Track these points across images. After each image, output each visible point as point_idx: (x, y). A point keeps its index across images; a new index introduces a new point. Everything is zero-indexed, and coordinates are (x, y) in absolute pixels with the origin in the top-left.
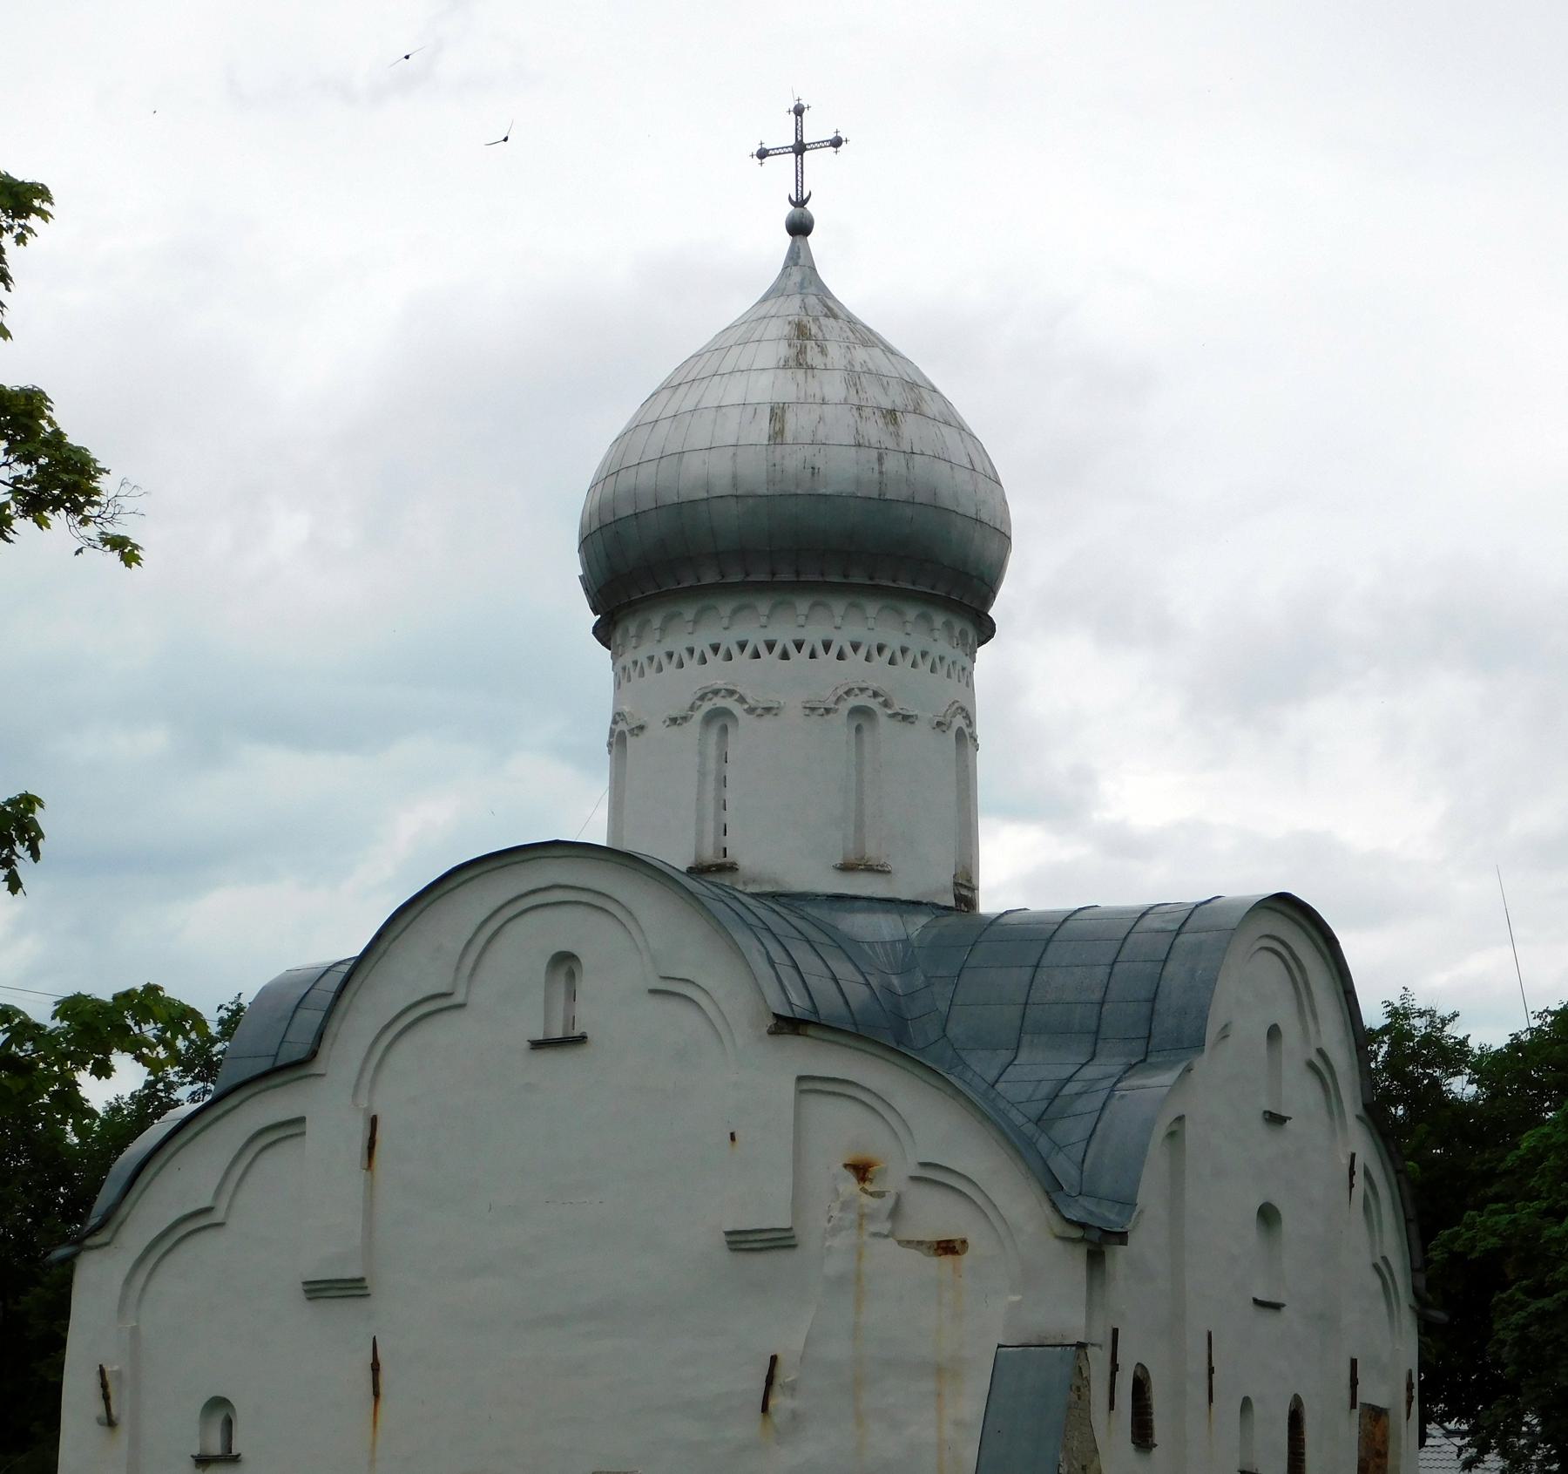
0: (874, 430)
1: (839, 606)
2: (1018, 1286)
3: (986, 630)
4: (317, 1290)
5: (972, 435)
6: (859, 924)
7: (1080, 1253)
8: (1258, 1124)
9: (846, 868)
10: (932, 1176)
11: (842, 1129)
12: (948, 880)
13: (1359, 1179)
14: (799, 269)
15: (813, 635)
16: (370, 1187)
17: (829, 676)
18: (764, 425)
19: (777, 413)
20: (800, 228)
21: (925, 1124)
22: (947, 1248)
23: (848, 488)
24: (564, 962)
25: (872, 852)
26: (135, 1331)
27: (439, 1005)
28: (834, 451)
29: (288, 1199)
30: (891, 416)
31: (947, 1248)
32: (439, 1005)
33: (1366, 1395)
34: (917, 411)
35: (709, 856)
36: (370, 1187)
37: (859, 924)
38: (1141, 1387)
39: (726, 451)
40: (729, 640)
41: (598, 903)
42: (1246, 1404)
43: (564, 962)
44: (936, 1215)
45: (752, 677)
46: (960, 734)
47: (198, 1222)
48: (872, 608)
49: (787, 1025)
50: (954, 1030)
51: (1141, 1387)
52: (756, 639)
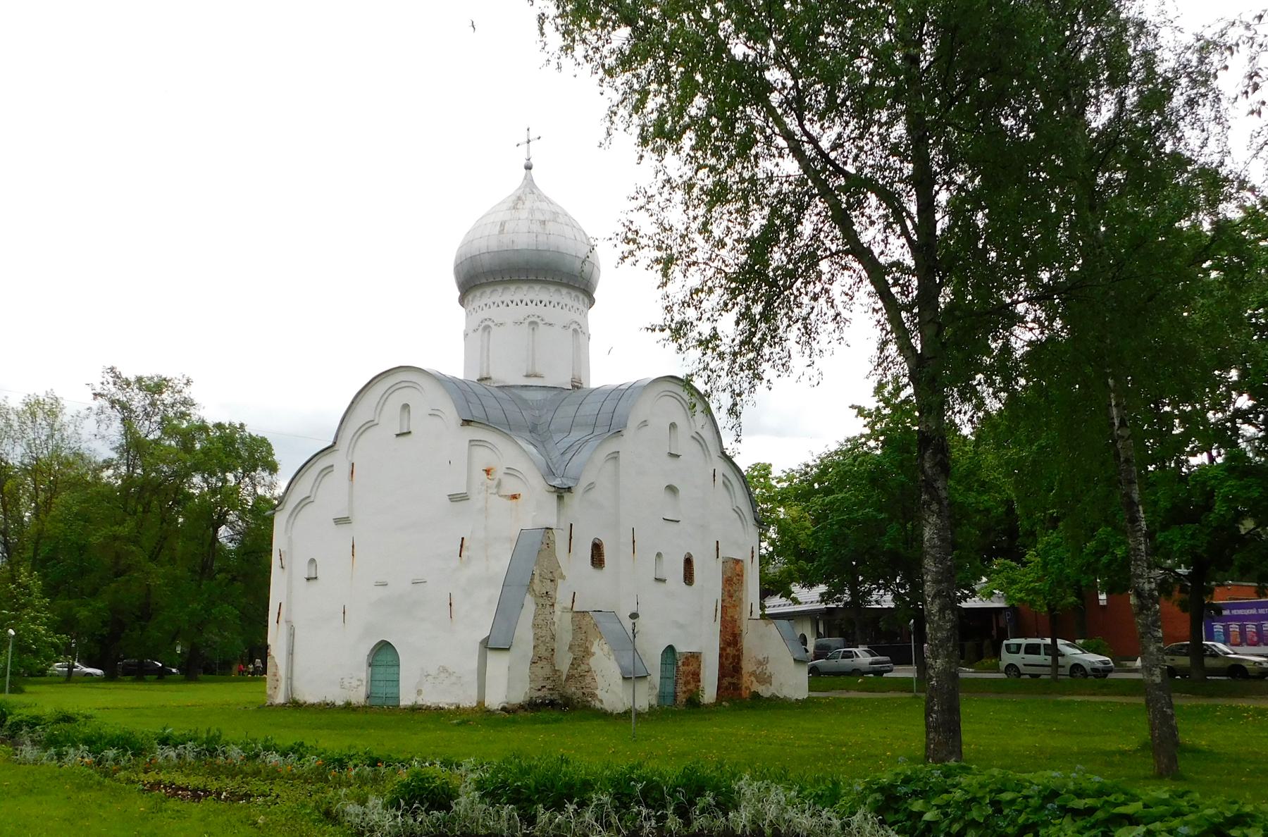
0: (536, 227)
1: (525, 287)
2: (538, 510)
3: (592, 302)
4: (338, 521)
5: (580, 229)
6: (528, 395)
7: (555, 496)
8: (669, 459)
9: (527, 376)
10: (510, 472)
11: (483, 457)
12: (569, 379)
13: (719, 479)
14: (529, 184)
15: (517, 298)
16: (351, 487)
17: (523, 311)
18: (498, 228)
19: (503, 224)
20: (528, 167)
21: (513, 457)
22: (514, 497)
23: (525, 247)
24: (406, 406)
25: (538, 370)
26: (290, 538)
27: (370, 425)
28: (522, 237)
29: (332, 495)
30: (544, 222)
31: (514, 497)
32: (370, 425)
33: (728, 552)
34: (555, 221)
35: (485, 375)
36: (351, 487)
37: (528, 395)
38: (597, 549)
39: (490, 242)
40: (490, 302)
41: (413, 386)
42: (659, 555)
43: (406, 406)
44: (511, 486)
45: (495, 313)
46: (575, 330)
47: (306, 501)
48: (537, 287)
49: (467, 422)
50: (552, 427)
51: (597, 549)
52: (498, 300)
